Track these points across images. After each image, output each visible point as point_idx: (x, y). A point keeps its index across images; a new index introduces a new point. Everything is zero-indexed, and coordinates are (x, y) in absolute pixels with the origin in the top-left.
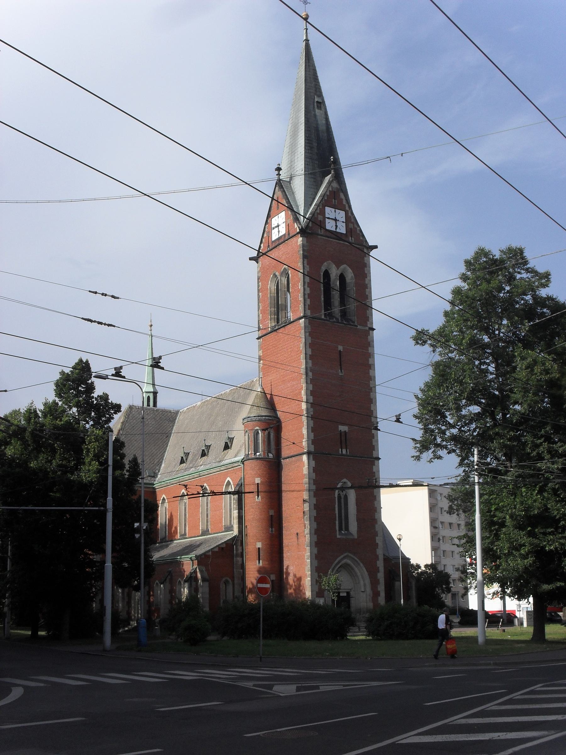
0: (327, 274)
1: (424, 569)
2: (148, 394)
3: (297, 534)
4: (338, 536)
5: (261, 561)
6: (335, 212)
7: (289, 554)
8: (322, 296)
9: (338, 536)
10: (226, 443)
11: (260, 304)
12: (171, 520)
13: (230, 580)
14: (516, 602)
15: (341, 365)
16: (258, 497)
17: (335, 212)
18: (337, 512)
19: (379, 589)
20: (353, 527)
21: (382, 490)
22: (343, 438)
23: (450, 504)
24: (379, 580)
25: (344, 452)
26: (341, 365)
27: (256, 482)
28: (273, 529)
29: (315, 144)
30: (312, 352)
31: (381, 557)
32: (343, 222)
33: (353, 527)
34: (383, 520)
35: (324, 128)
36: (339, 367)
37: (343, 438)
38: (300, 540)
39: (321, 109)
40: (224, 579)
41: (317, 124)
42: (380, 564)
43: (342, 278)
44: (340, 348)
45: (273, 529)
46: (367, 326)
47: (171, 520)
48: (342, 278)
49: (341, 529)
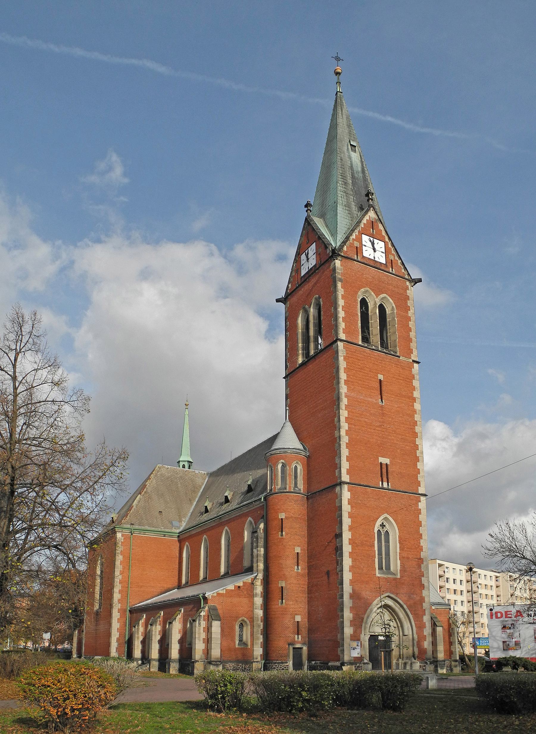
0: (364, 302)
2: (184, 463)
4: (378, 575)
6: (374, 258)
7: (317, 594)
8: (359, 322)
9: (378, 575)
11: (288, 343)
14: (196, 665)
16: (298, 565)
17: (374, 258)
18: (376, 548)
20: (396, 565)
21: (371, 623)
22: (384, 471)
25: (385, 485)
27: (296, 551)
30: (347, 377)
32: (382, 252)
33: (396, 565)
36: (380, 396)
37: (384, 471)
38: (331, 578)
43: (382, 308)
44: (381, 377)
46: (410, 358)
48: (382, 308)
49: (380, 568)
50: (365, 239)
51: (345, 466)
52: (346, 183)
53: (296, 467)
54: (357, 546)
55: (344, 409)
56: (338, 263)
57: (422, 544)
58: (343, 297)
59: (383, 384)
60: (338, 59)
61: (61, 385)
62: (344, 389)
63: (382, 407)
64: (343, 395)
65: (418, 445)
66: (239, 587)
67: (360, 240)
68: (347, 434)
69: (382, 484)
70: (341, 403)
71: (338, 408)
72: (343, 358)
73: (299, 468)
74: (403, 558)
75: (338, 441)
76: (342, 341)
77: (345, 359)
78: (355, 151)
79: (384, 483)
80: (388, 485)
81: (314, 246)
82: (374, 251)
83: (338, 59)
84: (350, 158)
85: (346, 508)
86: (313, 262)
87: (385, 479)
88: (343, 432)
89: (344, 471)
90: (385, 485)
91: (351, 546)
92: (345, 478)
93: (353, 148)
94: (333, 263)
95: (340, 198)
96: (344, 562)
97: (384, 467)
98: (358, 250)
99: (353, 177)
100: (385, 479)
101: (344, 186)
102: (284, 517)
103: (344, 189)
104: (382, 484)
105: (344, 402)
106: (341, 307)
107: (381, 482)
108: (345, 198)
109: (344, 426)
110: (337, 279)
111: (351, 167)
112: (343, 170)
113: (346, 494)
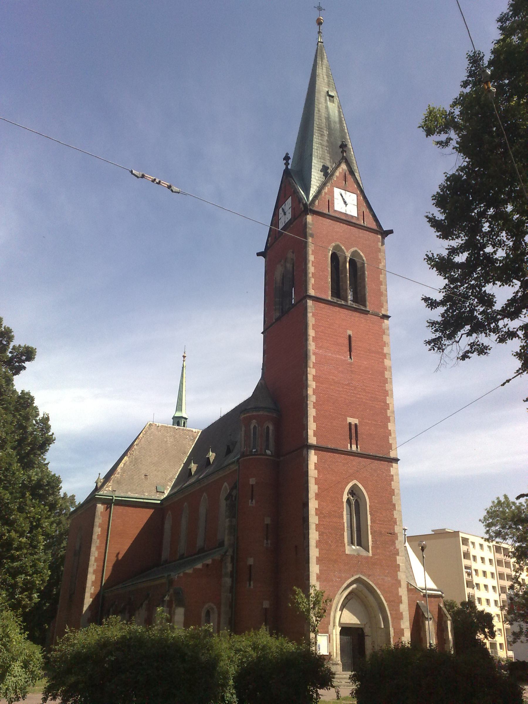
1: (461, 607)
3: (296, 547)
5: (252, 583)
10: (228, 446)
12: (48, 463)
13: (216, 609)
15: (350, 351)
16: (252, 501)
19: (402, 627)
22: (353, 431)
23: (488, 529)
24: (402, 613)
26: (350, 351)
28: (269, 541)
29: (326, 133)
31: (404, 584)
34: (256, 377)
35: (337, 119)
36: (349, 353)
37: (353, 431)
39: (334, 103)
40: (206, 606)
41: (328, 115)
42: (403, 592)
44: (350, 332)
45: (269, 541)
47: (48, 463)
50: (337, 191)
51: (312, 426)
52: (322, 135)
53: (268, 427)
54: (325, 517)
55: (312, 366)
56: (309, 218)
57: (395, 516)
58: (314, 252)
59: (353, 339)
60: (320, 9)
61: (251, 643)
62: (312, 346)
63: (351, 364)
64: (311, 352)
65: (388, 404)
66: (208, 565)
67: (332, 193)
68: (314, 393)
69: (351, 447)
70: (309, 361)
71: (306, 366)
72: (311, 314)
73: (271, 427)
74: (375, 531)
75: (306, 401)
76: (311, 297)
77: (313, 315)
78: (333, 102)
79: (353, 446)
80: (357, 447)
81: (289, 200)
82: (345, 202)
83: (320, 9)
84: (327, 108)
85: (313, 472)
86: (289, 216)
87: (354, 441)
88: (310, 391)
89: (311, 433)
90: (354, 448)
91: (317, 517)
92: (312, 440)
93: (332, 99)
94: (304, 218)
95: (316, 151)
96: (311, 536)
97: (353, 428)
98: (330, 203)
99: (329, 128)
100: (354, 441)
101: (320, 138)
102: (254, 483)
103: (321, 142)
104: (351, 447)
105: (312, 359)
106: (311, 262)
107: (349, 445)
108: (321, 149)
109: (312, 384)
110: (308, 235)
111: (328, 118)
112: (320, 121)
113: (313, 458)
